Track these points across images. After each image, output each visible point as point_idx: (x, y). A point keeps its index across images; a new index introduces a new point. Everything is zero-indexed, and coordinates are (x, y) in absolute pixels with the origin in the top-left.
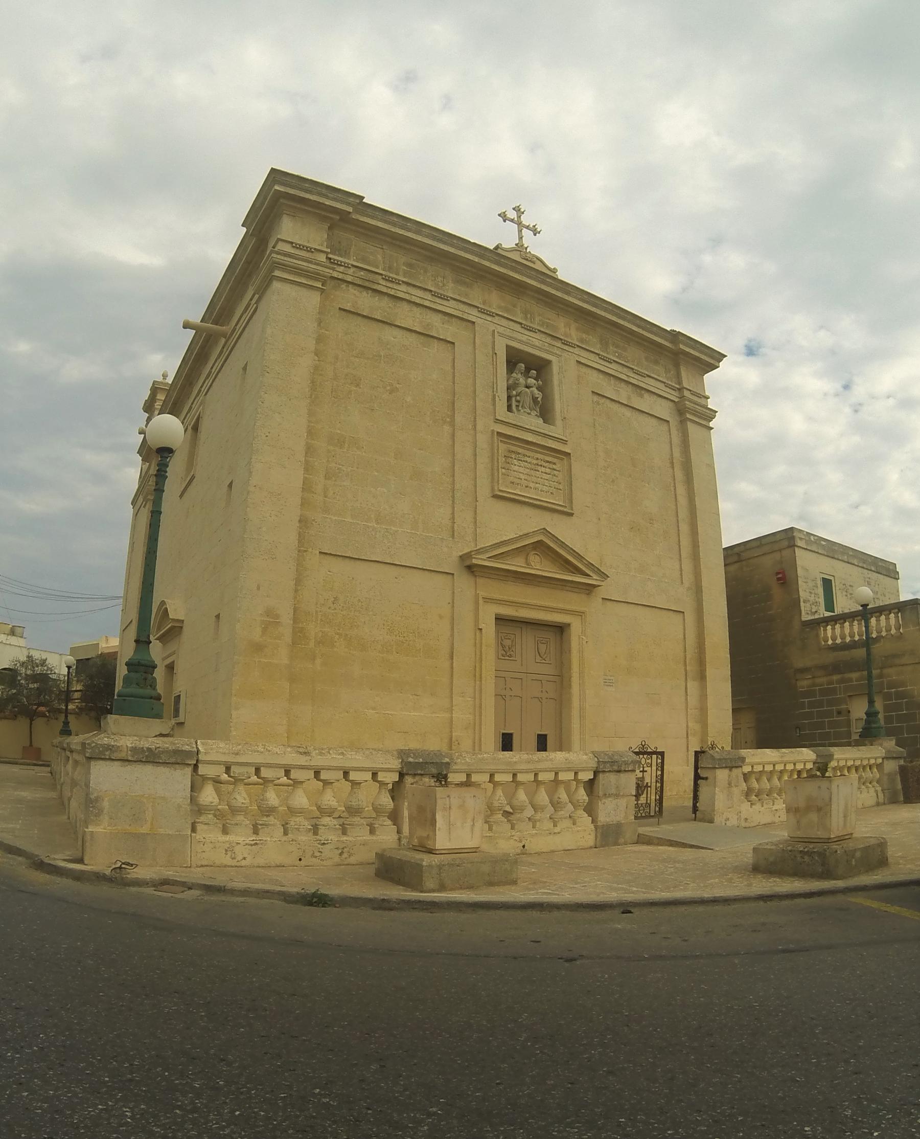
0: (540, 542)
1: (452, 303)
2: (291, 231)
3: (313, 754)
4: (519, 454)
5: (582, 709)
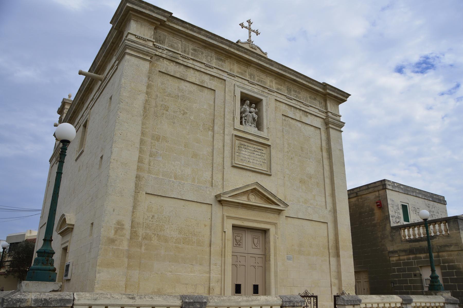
0: (255, 189)
1: (215, 70)
2: (135, 29)
3: (137, 299)
5: (276, 272)
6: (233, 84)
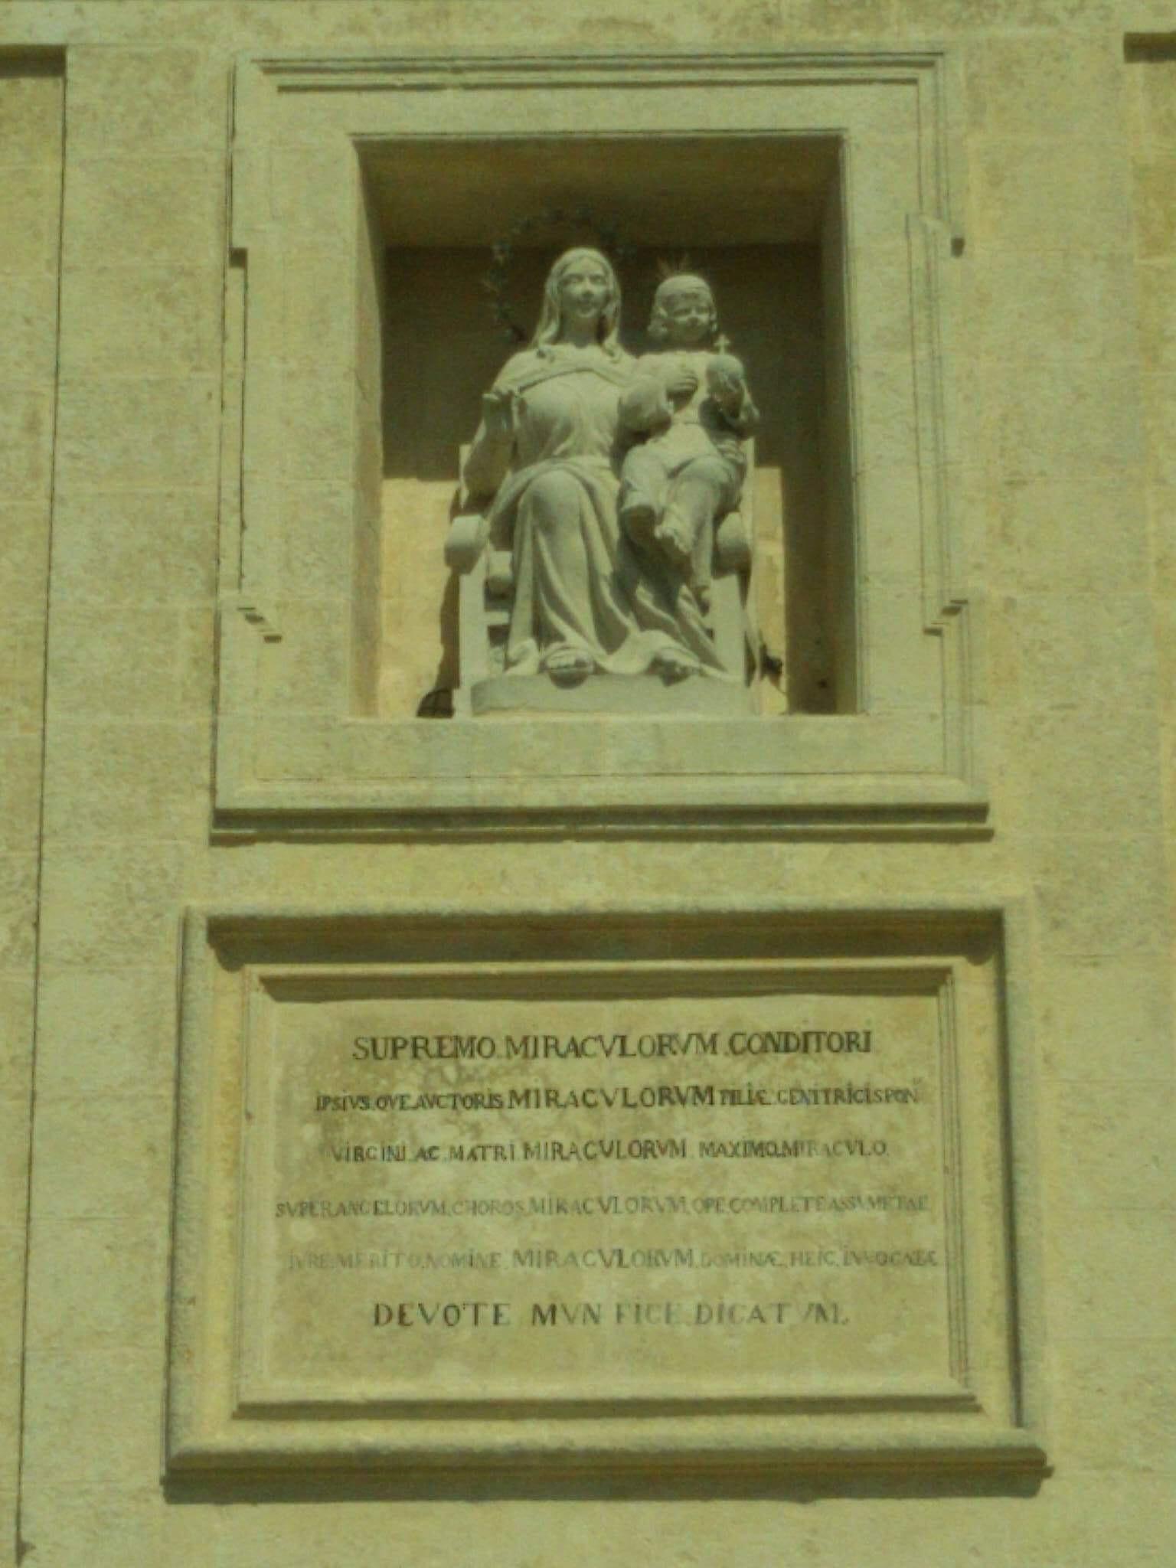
4: (472, 1046)
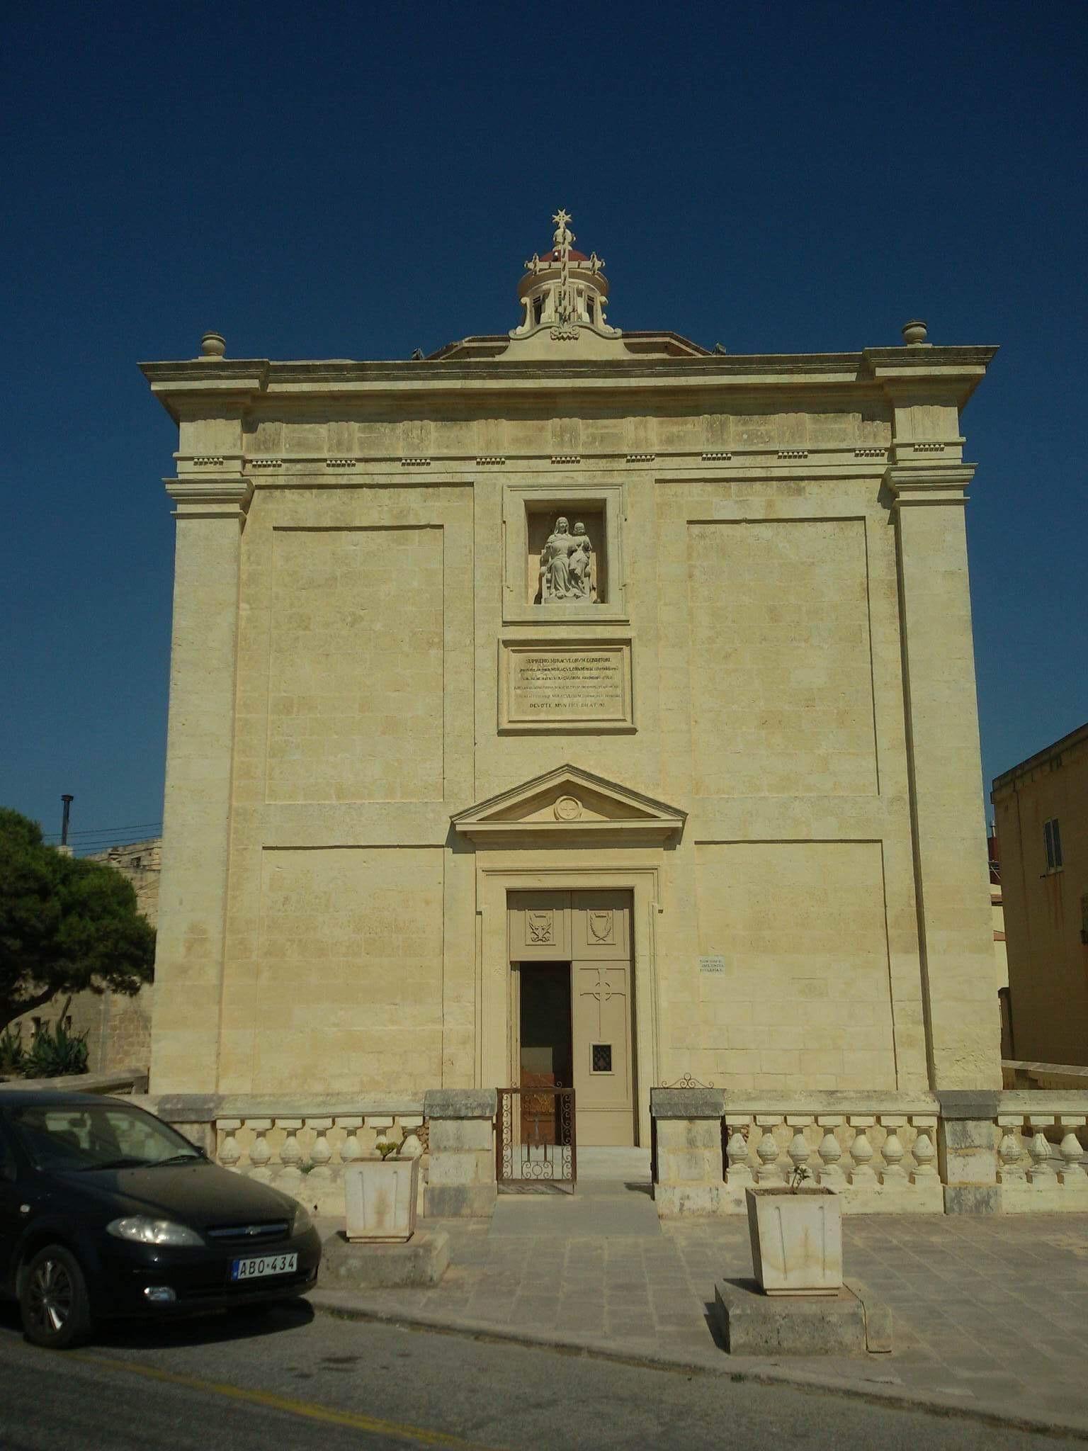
4: (545, 661)
6: (498, 488)
